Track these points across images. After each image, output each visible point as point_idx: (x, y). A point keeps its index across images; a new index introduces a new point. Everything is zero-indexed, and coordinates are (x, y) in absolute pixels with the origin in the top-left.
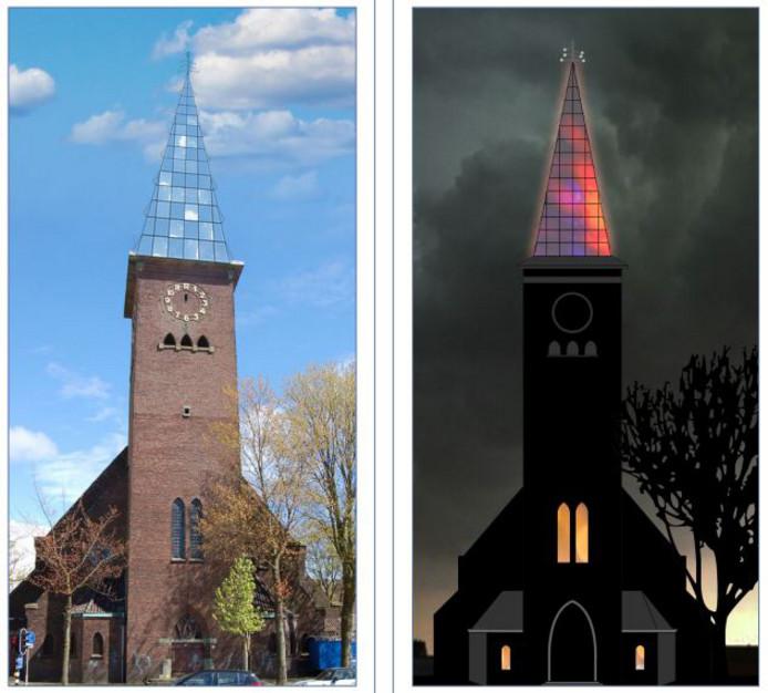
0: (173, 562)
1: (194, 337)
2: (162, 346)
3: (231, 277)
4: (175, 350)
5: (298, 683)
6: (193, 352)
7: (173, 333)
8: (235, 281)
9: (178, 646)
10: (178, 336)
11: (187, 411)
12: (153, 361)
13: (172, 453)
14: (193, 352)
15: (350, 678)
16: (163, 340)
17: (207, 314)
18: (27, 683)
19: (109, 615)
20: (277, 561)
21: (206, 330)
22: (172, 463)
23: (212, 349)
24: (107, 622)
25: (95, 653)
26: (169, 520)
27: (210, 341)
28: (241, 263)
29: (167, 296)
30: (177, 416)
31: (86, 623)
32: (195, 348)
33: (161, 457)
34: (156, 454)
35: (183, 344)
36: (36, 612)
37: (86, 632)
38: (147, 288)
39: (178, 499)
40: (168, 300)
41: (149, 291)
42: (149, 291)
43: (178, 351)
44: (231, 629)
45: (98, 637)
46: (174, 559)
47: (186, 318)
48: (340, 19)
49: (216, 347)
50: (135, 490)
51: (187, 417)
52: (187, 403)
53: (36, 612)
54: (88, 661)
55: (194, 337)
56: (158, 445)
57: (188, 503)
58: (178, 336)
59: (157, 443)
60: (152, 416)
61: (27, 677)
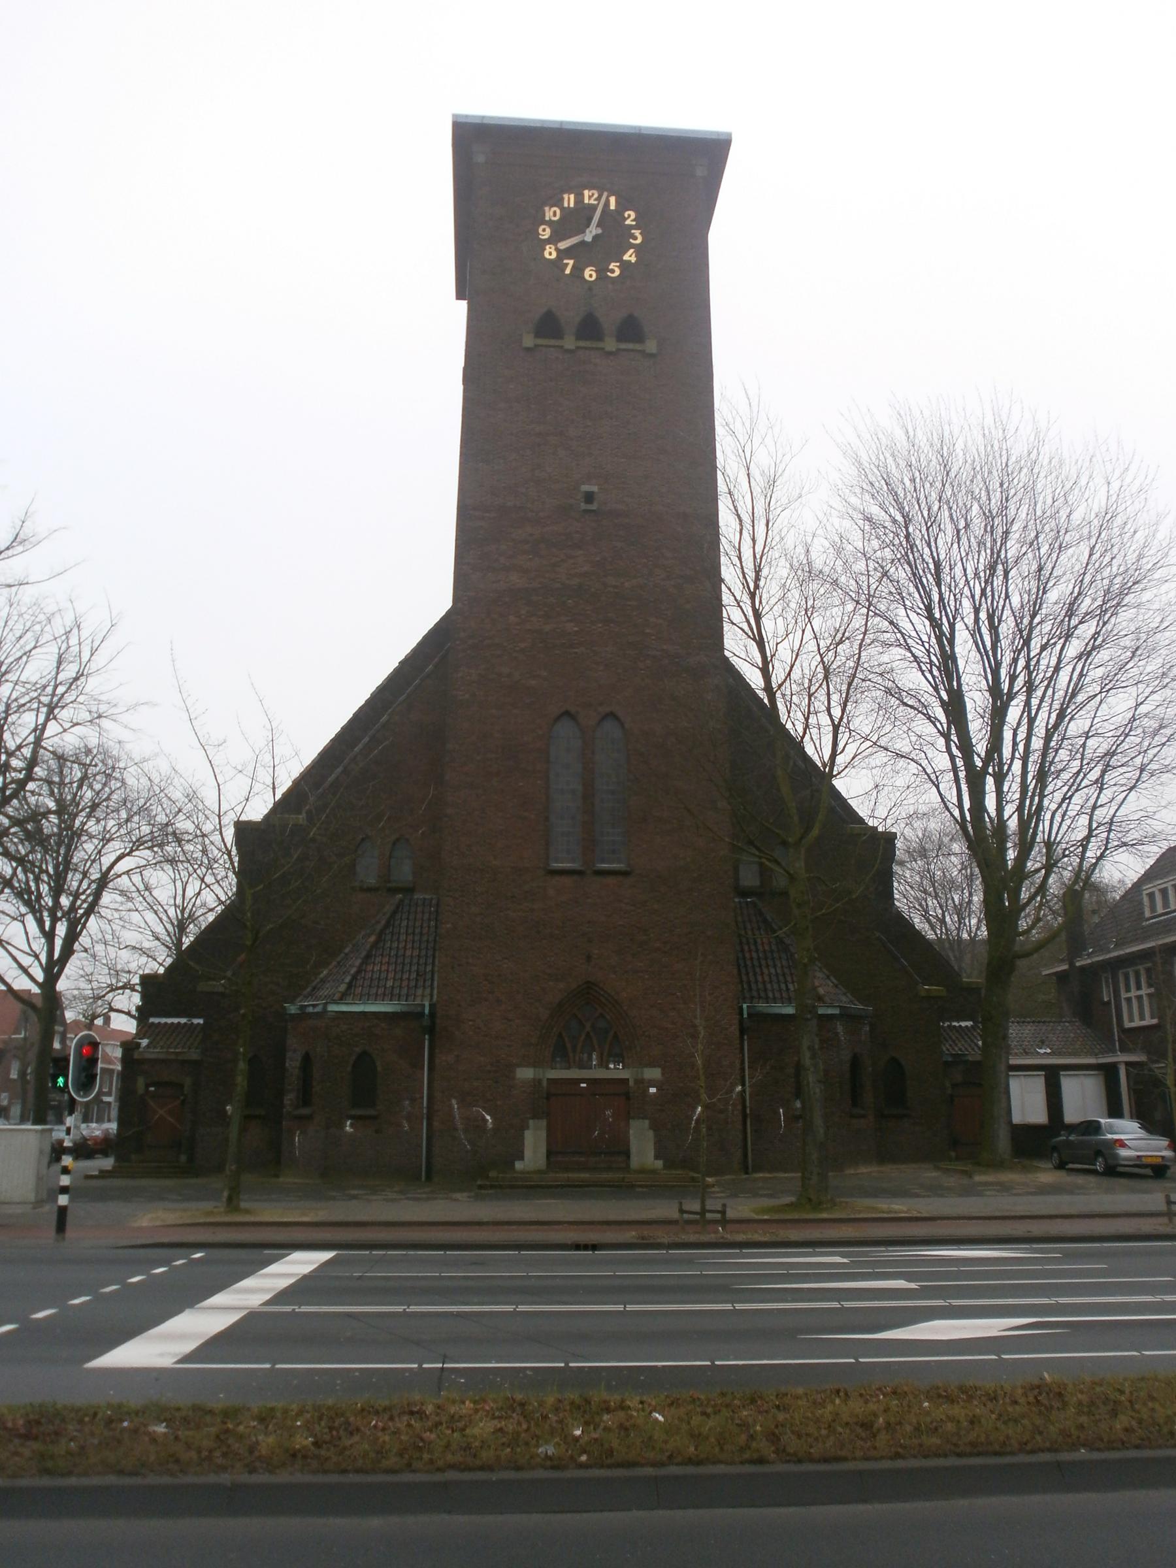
2: (529, 341)
11: (589, 497)
23: (651, 346)
32: (610, 344)
55: (609, 320)
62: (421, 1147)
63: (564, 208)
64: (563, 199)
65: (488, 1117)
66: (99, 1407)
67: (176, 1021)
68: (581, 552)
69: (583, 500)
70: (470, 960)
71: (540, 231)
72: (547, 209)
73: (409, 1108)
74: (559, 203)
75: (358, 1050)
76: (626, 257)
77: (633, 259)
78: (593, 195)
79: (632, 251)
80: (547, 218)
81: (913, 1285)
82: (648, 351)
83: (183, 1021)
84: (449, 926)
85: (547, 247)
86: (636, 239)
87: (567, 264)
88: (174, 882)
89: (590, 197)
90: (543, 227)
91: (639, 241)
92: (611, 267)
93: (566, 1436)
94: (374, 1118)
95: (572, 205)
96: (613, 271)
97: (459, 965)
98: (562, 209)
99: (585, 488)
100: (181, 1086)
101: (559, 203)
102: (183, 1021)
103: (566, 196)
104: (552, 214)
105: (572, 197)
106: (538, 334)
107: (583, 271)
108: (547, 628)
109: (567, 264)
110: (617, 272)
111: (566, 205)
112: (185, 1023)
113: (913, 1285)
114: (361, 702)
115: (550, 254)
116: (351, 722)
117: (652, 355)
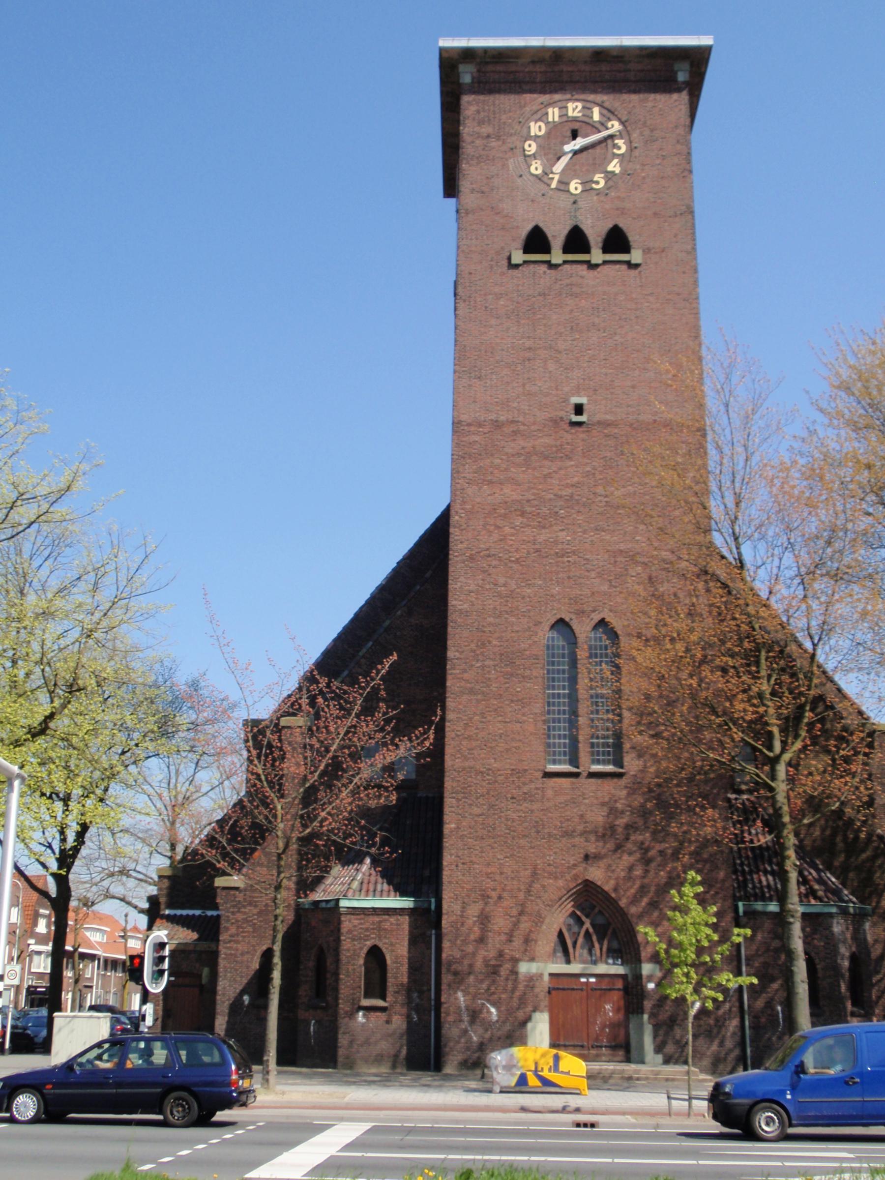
0: (548, 775)
1: (595, 234)
2: (518, 257)
3: (682, 77)
4: (551, 266)
5: (290, 1082)
6: (592, 266)
7: (541, 225)
8: (694, 88)
9: (564, 983)
10: (557, 235)
11: (579, 409)
12: (498, 296)
13: (545, 510)
14: (592, 266)
15: (676, 1062)
16: (520, 243)
17: (624, 172)
18: (653, 1063)
19: (406, 903)
20: (781, 769)
21: (622, 212)
22: (544, 536)
23: (636, 256)
24: (405, 920)
25: (367, 995)
26: (539, 672)
27: (632, 237)
28: (705, 40)
29: (528, 137)
30: (556, 422)
31: (347, 924)
32: (597, 256)
33: (518, 521)
34: (505, 516)
35: (567, 249)
36: (240, 897)
37: (346, 944)
38: (481, 123)
39: (561, 621)
40: (531, 148)
41: (486, 130)
42: (486, 130)
43: (556, 266)
44: (675, 934)
45: (376, 956)
46: (552, 768)
47: (575, 187)
48: (579, 133)
49: (647, 251)
50: (457, 602)
51: (580, 424)
52: (577, 391)
53: (240, 897)
54: (352, 1015)
55: (595, 234)
56: (509, 492)
57: (583, 629)
58: (557, 235)
59: (507, 490)
60: (497, 425)
61: (744, 969)
62: (429, 1036)
63: (549, 123)
64: (547, 114)
65: (493, 1010)
66: (474, 1168)
67: (191, 912)
68: (573, 463)
69: (573, 412)
70: (474, 859)
71: (526, 147)
72: (532, 124)
73: (418, 1000)
74: (543, 117)
75: (369, 943)
76: (610, 168)
77: (617, 170)
78: (577, 107)
79: (616, 161)
80: (532, 134)
81: (852, 1156)
82: (633, 262)
83: (198, 912)
84: (453, 826)
85: (534, 162)
86: (619, 148)
87: (553, 178)
88: (168, 767)
89: (574, 110)
90: (528, 143)
91: (623, 150)
92: (595, 179)
93: (874, 428)
94: (383, 1009)
95: (556, 119)
96: (597, 183)
97: (463, 864)
98: (547, 123)
99: (575, 400)
100: (200, 976)
101: (543, 117)
102: (198, 912)
103: (550, 110)
104: (537, 129)
105: (556, 110)
106: (527, 250)
107: (568, 184)
108: (541, 538)
109: (553, 178)
110: (602, 183)
111: (550, 119)
112: (200, 916)
113: (852, 1156)
114: (362, 602)
115: (536, 169)
116: (352, 621)
117: (637, 266)
